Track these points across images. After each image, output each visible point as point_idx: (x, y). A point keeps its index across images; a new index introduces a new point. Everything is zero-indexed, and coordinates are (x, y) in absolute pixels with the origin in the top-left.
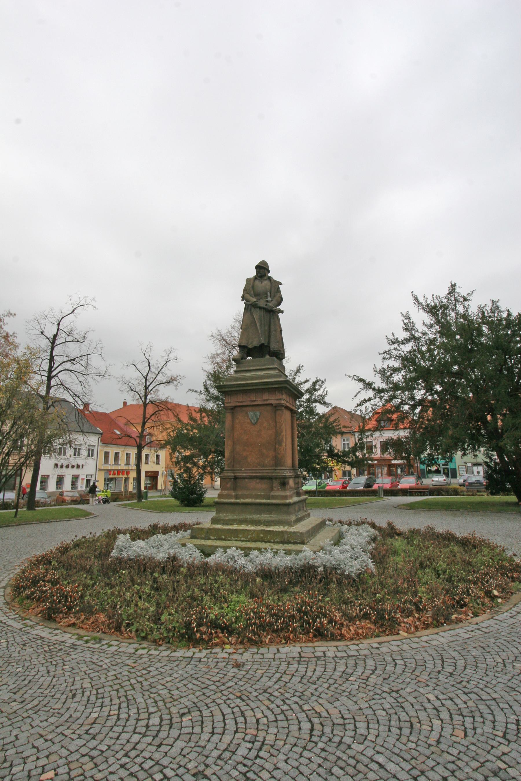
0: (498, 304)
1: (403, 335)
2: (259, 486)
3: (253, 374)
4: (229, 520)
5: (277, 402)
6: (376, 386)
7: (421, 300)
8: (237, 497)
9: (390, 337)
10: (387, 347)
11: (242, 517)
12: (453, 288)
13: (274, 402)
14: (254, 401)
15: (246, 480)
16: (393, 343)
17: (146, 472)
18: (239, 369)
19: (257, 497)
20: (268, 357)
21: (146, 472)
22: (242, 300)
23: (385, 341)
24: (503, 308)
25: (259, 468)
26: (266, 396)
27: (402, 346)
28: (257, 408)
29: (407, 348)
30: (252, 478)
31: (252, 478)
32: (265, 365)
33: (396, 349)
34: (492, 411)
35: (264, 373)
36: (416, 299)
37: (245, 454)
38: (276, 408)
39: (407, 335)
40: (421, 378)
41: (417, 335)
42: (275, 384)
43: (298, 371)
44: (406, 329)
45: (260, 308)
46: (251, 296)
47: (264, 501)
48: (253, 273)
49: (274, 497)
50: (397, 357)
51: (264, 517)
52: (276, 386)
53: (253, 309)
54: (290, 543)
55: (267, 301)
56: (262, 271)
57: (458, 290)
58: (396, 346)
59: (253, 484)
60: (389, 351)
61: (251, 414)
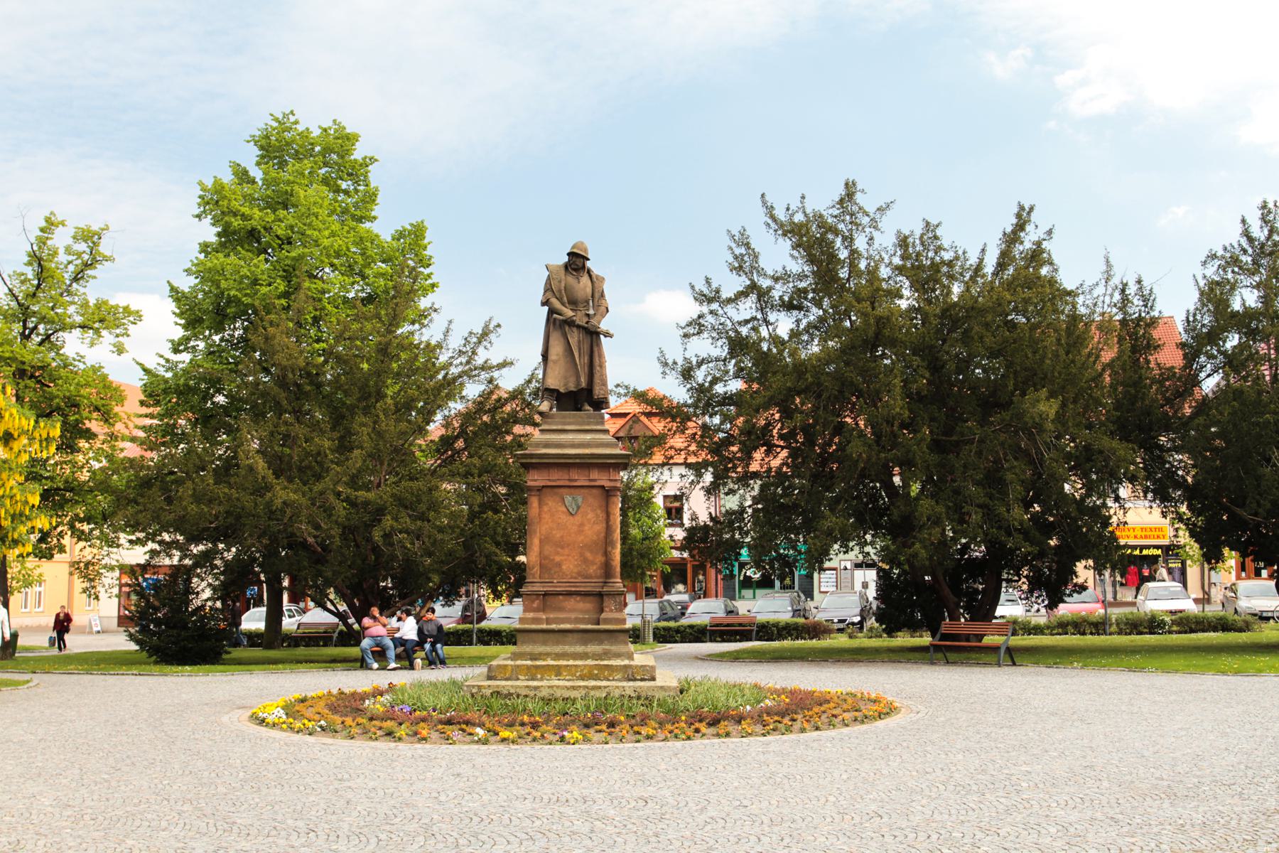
0: (938, 233)
1: (732, 284)
2: (581, 605)
3: (570, 436)
4: (540, 654)
5: (612, 484)
6: (480, 350)
7: (781, 215)
8: (548, 621)
9: (701, 286)
11: (558, 649)
12: (850, 191)
13: (607, 484)
16: (710, 301)
19: (577, 621)
24: (946, 243)
25: (580, 579)
26: (595, 474)
27: (730, 310)
28: (577, 490)
30: (569, 594)
31: (569, 594)
32: (588, 424)
34: (907, 464)
35: (588, 437)
37: (558, 559)
38: (608, 493)
39: (740, 283)
40: (776, 405)
41: (765, 283)
44: (739, 269)
45: (579, 327)
46: (563, 304)
47: (590, 627)
49: (607, 621)
50: (720, 332)
51: (591, 648)
54: (635, 680)
55: (588, 315)
56: (579, 262)
57: (859, 197)
58: (715, 306)
59: (571, 603)
60: (700, 317)
61: (568, 499)
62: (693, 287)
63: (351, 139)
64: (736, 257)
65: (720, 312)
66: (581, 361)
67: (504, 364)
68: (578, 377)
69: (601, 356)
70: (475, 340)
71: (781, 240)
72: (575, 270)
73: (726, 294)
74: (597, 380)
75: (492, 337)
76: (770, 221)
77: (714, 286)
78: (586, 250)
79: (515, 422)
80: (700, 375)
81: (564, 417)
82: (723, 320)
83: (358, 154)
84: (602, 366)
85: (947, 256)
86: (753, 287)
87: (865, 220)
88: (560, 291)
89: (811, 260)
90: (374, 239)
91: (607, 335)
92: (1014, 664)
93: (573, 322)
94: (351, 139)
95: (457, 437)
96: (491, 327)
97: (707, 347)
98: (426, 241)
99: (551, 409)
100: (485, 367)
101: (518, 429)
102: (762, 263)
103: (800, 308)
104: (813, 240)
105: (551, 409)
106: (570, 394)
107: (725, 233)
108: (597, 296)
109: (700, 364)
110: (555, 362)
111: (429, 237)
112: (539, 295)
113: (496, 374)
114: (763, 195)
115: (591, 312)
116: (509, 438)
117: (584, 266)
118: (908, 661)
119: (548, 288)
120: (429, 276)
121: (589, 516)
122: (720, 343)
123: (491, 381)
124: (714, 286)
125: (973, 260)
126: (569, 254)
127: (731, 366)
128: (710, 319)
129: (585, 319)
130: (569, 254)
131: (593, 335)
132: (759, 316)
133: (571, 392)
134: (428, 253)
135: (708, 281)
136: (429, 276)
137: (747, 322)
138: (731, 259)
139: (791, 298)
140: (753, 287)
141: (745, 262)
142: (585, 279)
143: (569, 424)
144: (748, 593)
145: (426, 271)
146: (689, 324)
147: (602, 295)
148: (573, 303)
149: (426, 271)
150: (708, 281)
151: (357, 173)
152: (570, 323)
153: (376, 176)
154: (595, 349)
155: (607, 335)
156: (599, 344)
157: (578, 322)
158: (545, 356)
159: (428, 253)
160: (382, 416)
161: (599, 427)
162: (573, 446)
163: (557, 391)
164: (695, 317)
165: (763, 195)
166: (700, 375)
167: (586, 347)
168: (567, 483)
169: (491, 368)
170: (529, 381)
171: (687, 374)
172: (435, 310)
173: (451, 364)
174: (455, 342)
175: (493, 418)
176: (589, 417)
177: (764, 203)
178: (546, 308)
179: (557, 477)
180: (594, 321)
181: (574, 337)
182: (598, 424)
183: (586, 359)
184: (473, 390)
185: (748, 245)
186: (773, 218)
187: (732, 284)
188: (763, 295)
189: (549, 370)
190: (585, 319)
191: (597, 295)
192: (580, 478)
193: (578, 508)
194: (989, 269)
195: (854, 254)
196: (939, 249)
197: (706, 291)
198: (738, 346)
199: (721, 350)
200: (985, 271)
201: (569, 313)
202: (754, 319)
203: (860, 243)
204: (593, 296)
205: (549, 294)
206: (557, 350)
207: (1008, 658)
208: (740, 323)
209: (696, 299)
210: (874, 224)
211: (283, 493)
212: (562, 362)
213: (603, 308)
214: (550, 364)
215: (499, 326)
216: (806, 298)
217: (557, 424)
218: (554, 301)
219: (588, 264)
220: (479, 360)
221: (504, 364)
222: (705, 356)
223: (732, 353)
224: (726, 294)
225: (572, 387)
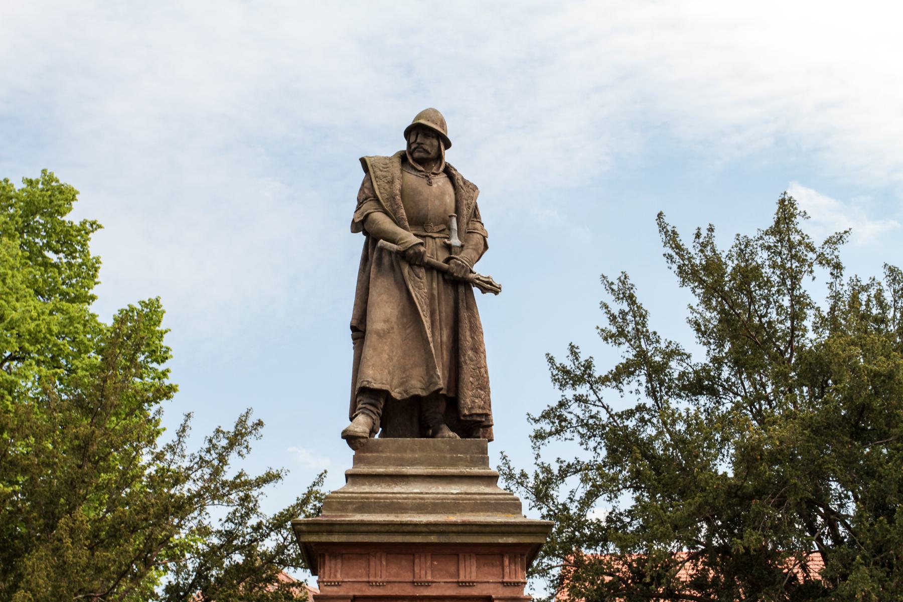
1: (608, 357)
3: (415, 488)
6: (233, 457)
7: (687, 241)
10: (552, 396)
12: (786, 212)
14: (428, 584)
16: (577, 380)
18: (364, 469)
20: (448, 433)
23: (546, 372)
27: (608, 394)
29: (632, 394)
32: (454, 463)
35: (455, 489)
39: (623, 353)
42: (458, 533)
43: (237, 438)
44: (616, 336)
45: (430, 268)
46: (398, 222)
50: (590, 428)
52: (510, 540)
53: (406, 270)
55: (449, 247)
56: (430, 144)
57: (800, 223)
58: (583, 389)
60: (562, 404)
62: (551, 360)
63: (68, 196)
64: (613, 319)
65: (593, 398)
66: (437, 338)
67: (270, 478)
68: (429, 367)
69: (475, 329)
70: (224, 442)
72: (420, 161)
73: (601, 369)
74: (468, 377)
75: (251, 440)
77: (582, 359)
78: (443, 124)
79: (283, 563)
81: (402, 449)
82: (594, 410)
83: (74, 217)
84: (477, 348)
86: (642, 359)
87: (811, 256)
88: (392, 197)
90: (89, 322)
91: (489, 287)
93: (420, 255)
94: (68, 196)
95: (193, 586)
96: (249, 423)
98: (162, 327)
99: (373, 432)
102: (651, 326)
104: (728, 289)
105: (373, 432)
107: (599, 280)
108: (465, 210)
109: (564, 473)
110: (381, 335)
112: (349, 211)
113: (254, 493)
114: (660, 215)
115: (455, 241)
116: (271, 588)
117: (439, 157)
119: (367, 195)
120: (164, 374)
122: (592, 443)
123: (246, 499)
124: (582, 359)
128: (576, 409)
131: (459, 285)
132: (650, 403)
133: (416, 398)
134: (165, 342)
135: (574, 351)
136: (164, 374)
138: (605, 323)
140: (642, 359)
141: (628, 322)
143: (412, 463)
145: (161, 368)
146: (546, 415)
147: (475, 214)
148: (419, 222)
149: (161, 368)
150: (574, 351)
151: (71, 240)
152: (411, 258)
153: (96, 245)
154: (464, 314)
155: (489, 287)
156: (471, 306)
157: (427, 258)
158: (359, 331)
159: (165, 342)
160: (68, 541)
161: (476, 470)
162: (422, 507)
163: (385, 394)
164: (554, 404)
165: (660, 215)
167: (445, 309)
169: (248, 484)
170: (305, 502)
173: (188, 477)
174: (195, 445)
175: (249, 555)
176: (454, 450)
177: (662, 227)
180: (463, 257)
181: (421, 288)
182: (473, 463)
183: (445, 335)
184: (216, 515)
185: (631, 299)
187: (608, 357)
188: (656, 372)
189: (368, 352)
191: (465, 212)
197: (569, 364)
198: (621, 443)
199: (593, 453)
201: (410, 238)
202: (641, 408)
204: (457, 210)
205: (368, 207)
206: (385, 310)
209: (555, 380)
212: (396, 337)
213: (477, 238)
214: (371, 340)
215: (260, 424)
217: (387, 462)
220: (229, 475)
221: (270, 478)
222: (572, 461)
223: (614, 458)
224: (601, 369)
225: (417, 387)
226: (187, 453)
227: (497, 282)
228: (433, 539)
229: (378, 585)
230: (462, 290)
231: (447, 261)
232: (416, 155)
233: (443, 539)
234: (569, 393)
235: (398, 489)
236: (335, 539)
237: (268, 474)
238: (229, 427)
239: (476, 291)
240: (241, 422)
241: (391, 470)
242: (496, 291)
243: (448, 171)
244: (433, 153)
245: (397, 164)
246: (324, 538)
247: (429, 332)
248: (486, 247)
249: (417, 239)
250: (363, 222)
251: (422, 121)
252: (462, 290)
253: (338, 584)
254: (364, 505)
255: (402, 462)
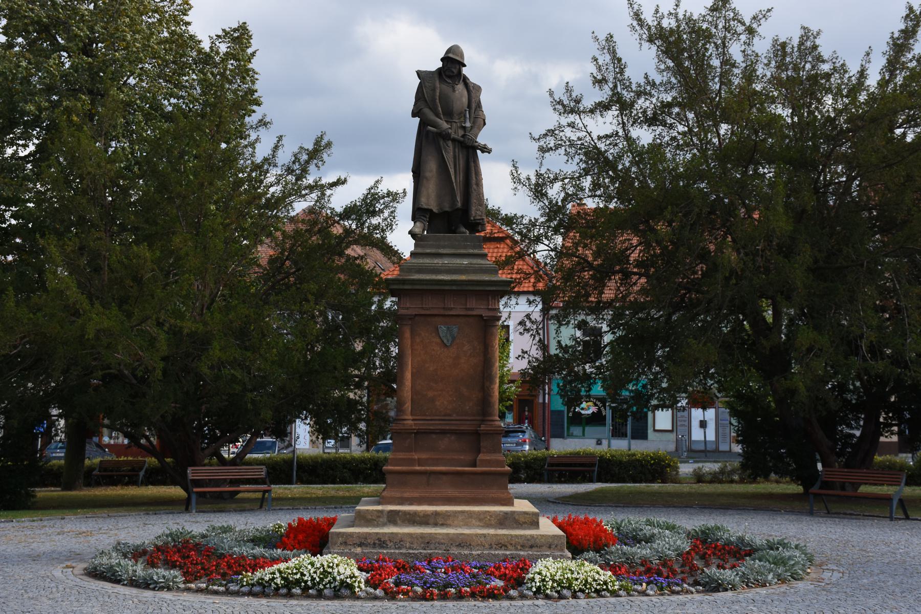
0: (818, 42)
6: (312, 168)
7: (648, 17)
9: (560, 94)
10: (551, 119)
13: (485, 314)
14: (451, 309)
15: (434, 436)
16: (572, 111)
17: (604, 425)
18: (420, 250)
21: (604, 425)
22: (414, 115)
24: (825, 51)
25: (454, 417)
26: (472, 303)
30: (443, 432)
31: (443, 432)
32: (465, 247)
33: (572, 125)
35: (465, 262)
36: (637, 16)
37: (430, 394)
39: (603, 95)
41: (627, 96)
44: (599, 82)
45: (454, 140)
48: (435, 64)
53: (441, 142)
55: (464, 128)
58: (572, 118)
61: (443, 329)
64: (599, 68)
66: (457, 179)
67: (340, 182)
69: (478, 173)
71: (646, 45)
76: (635, 23)
78: (462, 56)
80: (555, 192)
84: (479, 184)
85: (826, 67)
89: (679, 70)
92: (907, 518)
96: (323, 143)
97: (561, 163)
100: (316, 186)
101: (355, 251)
103: (664, 124)
104: (680, 44)
106: (444, 215)
111: (255, 44)
115: (468, 124)
117: (460, 72)
118: (792, 512)
121: (465, 348)
125: (853, 69)
126: (442, 60)
127: (587, 182)
129: (461, 132)
130: (442, 60)
137: (607, 137)
139: (655, 114)
142: (460, 87)
143: (444, 247)
144: (577, 430)
147: (479, 105)
154: (472, 164)
155: (485, 150)
157: (453, 136)
161: (476, 251)
163: (431, 211)
166: (555, 192)
167: (462, 163)
168: (442, 312)
171: (538, 192)
172: (265, 124)
174: (284, 157)
178: (417, 120)
179: (432, 305)
183: (461, 177)
186: (641, 22)
187: (593, 96)
190: (461, 132)
191: (474, 106)
192: (456, 307)
193: (454, 338)
194: (872, 81)
195: (728, 63)
196: (820, 59)
200: (868, 83)
203: (735, 51)
204: (469, 106)
206: (431, 167)
207: (901, 511)
208: (599, 138)
210: (751, 31)
211: (99, 319)
216: (670, 114)
217: (431, 247)
218: (427, 111)
219: (465, 71)
220: (310, 180)
221: (340, 182)
226: (280, 164)
227: (489, 146)
228: (454, 288)
229: (427, 309)
230: (471, 151)
231: (463, 136)
232: (447, 73)
233: (459, 288)
234: (564, 120)
235: (436, 261)
236: (406, 287)
237: (338, 180)
238: (310, 147)
239: (479, 152)
240: (318, 142)
241: (433, 251)
242: (489, 151)
243: (465, 80)
244: (455, 71)
245: (436, 76)
246: (401, 287)
247: (452, 171)
248: (485, 124)
249: (446, 109)
250: (418, 112)
251: (451, 55)
252: (471, 151)
253: (407, 309)
254: (420, 270)
255: (439, 247)
